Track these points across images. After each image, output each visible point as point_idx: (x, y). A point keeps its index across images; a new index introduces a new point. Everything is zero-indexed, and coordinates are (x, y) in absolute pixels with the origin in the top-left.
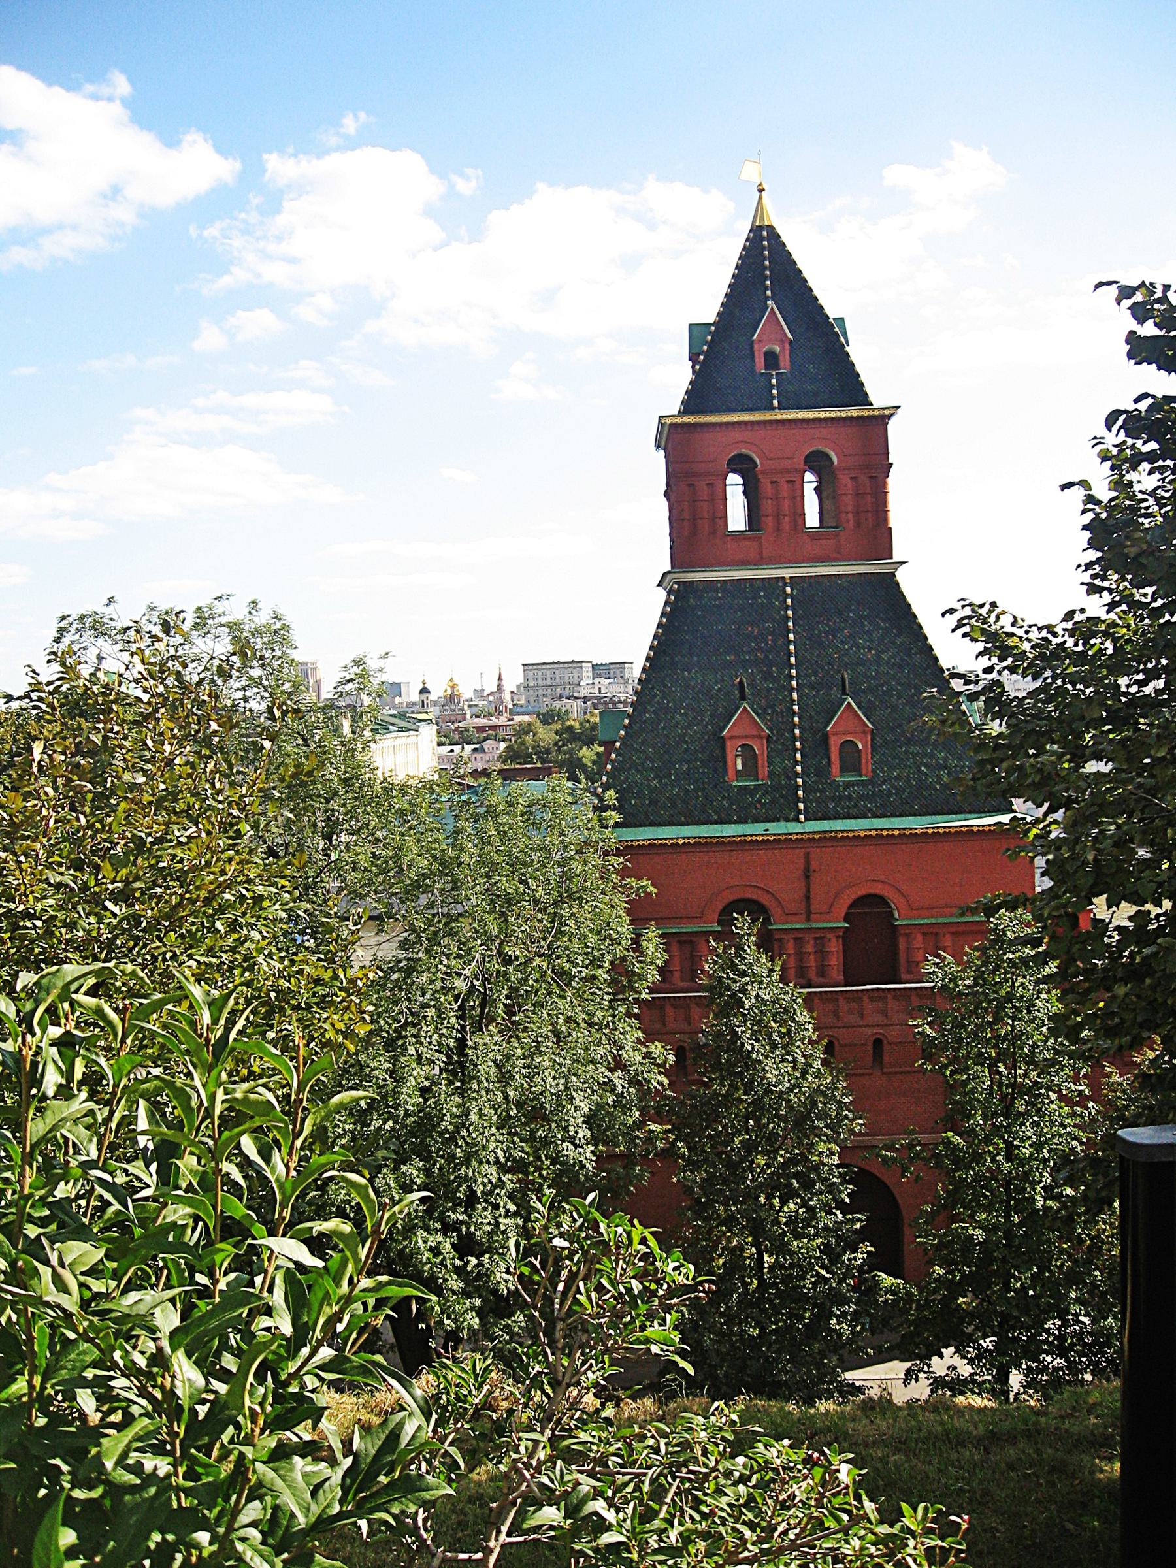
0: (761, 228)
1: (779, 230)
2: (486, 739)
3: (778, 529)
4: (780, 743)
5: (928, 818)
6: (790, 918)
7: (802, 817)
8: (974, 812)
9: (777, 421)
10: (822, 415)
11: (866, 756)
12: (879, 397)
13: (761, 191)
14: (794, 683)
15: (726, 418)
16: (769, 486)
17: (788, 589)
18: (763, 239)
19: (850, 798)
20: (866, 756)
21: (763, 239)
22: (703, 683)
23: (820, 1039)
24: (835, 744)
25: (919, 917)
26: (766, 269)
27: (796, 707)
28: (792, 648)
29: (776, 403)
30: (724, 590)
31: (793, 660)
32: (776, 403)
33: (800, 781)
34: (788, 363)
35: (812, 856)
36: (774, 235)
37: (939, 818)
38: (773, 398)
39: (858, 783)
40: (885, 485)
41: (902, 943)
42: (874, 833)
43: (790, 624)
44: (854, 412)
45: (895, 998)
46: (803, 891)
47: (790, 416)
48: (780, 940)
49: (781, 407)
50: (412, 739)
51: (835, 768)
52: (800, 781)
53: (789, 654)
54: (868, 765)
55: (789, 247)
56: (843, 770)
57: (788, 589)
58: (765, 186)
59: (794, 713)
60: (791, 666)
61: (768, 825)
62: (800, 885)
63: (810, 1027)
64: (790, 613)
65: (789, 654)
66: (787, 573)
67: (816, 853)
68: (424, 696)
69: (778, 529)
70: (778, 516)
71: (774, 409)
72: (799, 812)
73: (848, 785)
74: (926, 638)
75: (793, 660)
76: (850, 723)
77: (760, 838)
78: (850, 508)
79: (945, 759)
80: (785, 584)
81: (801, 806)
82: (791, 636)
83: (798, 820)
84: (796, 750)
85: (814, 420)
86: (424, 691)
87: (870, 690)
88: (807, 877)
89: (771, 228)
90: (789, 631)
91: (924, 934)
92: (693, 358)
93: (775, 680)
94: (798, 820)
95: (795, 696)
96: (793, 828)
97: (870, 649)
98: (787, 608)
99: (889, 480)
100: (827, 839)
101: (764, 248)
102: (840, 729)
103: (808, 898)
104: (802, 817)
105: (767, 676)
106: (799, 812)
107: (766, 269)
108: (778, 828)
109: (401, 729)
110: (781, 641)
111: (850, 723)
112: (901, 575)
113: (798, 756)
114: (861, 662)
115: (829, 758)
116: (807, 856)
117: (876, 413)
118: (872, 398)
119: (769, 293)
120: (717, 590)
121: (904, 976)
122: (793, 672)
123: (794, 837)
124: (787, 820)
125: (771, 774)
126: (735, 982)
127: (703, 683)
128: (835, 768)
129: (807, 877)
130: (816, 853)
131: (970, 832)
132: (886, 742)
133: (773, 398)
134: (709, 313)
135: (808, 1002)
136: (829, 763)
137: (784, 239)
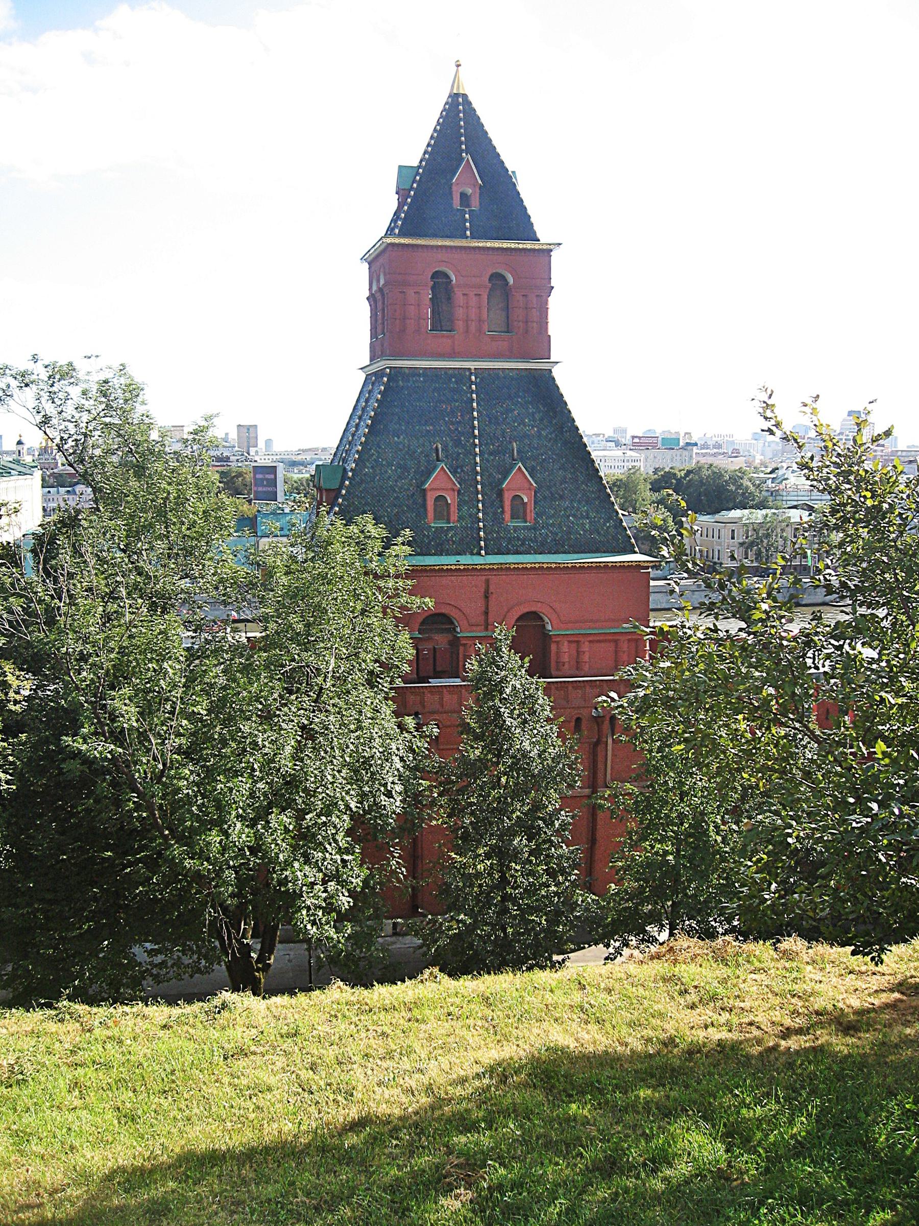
0: (457, 95)
1: (471, 98)
2: (77, 483)
3: (467, 331)
4: (466, 496)
5: (576, 556)
6: (475, 628)
7: (483, 552)
8: (608, 552)
9: (469, 248)
10: (505, 246)
11: (531, 507)
12: (545, 232)
13: (458, 66)
14: (477, 450)
15: (440, 242)
16: (462, 297)
17: (473, 378)
18: (459, 104)
19: (519, 539)
20: (531, 507)
21: (459, 104)
22: (409, 446)
23: (557, 717)
24: (507, 497)
25: (567, 629)
26: (460, 134)
27: (478, 468)
28: (476, 422)
29: (468, 233)
30: (424, 375)
31: (476, 432)
32: (468, 233)
33: (481, 524)
34: (478, 204)
35: (491, 582)
36: (467, 102)
37: (583, 555)
38: (466, 229)
39: (524, 528)
40: (546, 302)
41: (553, 647)
42: (537, 566)
43: (475, 405)
44: (528, 245)
45: (557, 688)
46: (483, 609)
47: (481, 245)
48: (465, 645)
49: (473, 237)
50: (29, 482)
51: (507, 516)
52: (481, 524)
53: (474, 427)
54: (531, 515)
55: (478, 113)
56: (513, 517)
57: (473, 378)
58: (461, 63)
59: (477, 472)
60: (475, 437)
61: (458, 558)
62: (481, 604)
63: (548, 708)
64: (474, 396)
65: (474, 427)
66: (472, 365)
67: (494, 579)
68: (20, 447)
69: (467, 331)
70: (467, 321)
71: (467, 237)
72: (481, 548)
73: (516, 529)
74: (573, 420)
75: (476, 432)
76: (519, 483)
77: (453, 567)
78: (521, 318)
79: (587, 512)
80: (471, 374)
81: (482, 543)
82: (475, 414)
83: (479, 554)
84: (478, 501)
85: (499, 249)
86: (20, 443)
87: (535, 458)
88: (487, 597)
89: (465, 96)
90: (473, 410)
91: (569, 642)
92: (401, 192)
93: (464, 446)
94: (479, 554)
95: (478, 459)
96: (477, 560)
97: (533, 427)
98: (472, 392)
99: (550, 299)
100: (504, 569)
101: (460, 111)
102: (434, 486)
103: (486, 613)
104: (483, 552)
105: (457, 443)
106: (481, 548)
107: (460, 134)
108: (466, 560)
109: (20, 473)
110: (467, 417)
111: (519, 483)
112: (557, 372)
113: (480, 505)
114: (525, 436)
115: (502, 507)
116: (487, 582)
117: (545, 247)
118: (539, 235)
119: (463, 147)
120: (419, 375)
121: (553, 673)
122: (477, 441)
123: (479, 567)
124: (472, 554)
125: (461, 518)
126: (497, 673)
127: (409, 446)
128: (507, 516)
129: (487, 597)
130: (494, 579)
131: (606, 567)
132: (545, 498)
133: (466, 229)
134: (413, 159)
135: (547, 691)
136: (503, 512)
137: (474, 105)
